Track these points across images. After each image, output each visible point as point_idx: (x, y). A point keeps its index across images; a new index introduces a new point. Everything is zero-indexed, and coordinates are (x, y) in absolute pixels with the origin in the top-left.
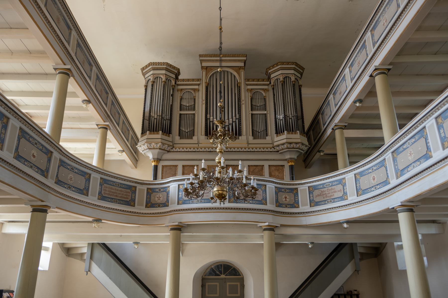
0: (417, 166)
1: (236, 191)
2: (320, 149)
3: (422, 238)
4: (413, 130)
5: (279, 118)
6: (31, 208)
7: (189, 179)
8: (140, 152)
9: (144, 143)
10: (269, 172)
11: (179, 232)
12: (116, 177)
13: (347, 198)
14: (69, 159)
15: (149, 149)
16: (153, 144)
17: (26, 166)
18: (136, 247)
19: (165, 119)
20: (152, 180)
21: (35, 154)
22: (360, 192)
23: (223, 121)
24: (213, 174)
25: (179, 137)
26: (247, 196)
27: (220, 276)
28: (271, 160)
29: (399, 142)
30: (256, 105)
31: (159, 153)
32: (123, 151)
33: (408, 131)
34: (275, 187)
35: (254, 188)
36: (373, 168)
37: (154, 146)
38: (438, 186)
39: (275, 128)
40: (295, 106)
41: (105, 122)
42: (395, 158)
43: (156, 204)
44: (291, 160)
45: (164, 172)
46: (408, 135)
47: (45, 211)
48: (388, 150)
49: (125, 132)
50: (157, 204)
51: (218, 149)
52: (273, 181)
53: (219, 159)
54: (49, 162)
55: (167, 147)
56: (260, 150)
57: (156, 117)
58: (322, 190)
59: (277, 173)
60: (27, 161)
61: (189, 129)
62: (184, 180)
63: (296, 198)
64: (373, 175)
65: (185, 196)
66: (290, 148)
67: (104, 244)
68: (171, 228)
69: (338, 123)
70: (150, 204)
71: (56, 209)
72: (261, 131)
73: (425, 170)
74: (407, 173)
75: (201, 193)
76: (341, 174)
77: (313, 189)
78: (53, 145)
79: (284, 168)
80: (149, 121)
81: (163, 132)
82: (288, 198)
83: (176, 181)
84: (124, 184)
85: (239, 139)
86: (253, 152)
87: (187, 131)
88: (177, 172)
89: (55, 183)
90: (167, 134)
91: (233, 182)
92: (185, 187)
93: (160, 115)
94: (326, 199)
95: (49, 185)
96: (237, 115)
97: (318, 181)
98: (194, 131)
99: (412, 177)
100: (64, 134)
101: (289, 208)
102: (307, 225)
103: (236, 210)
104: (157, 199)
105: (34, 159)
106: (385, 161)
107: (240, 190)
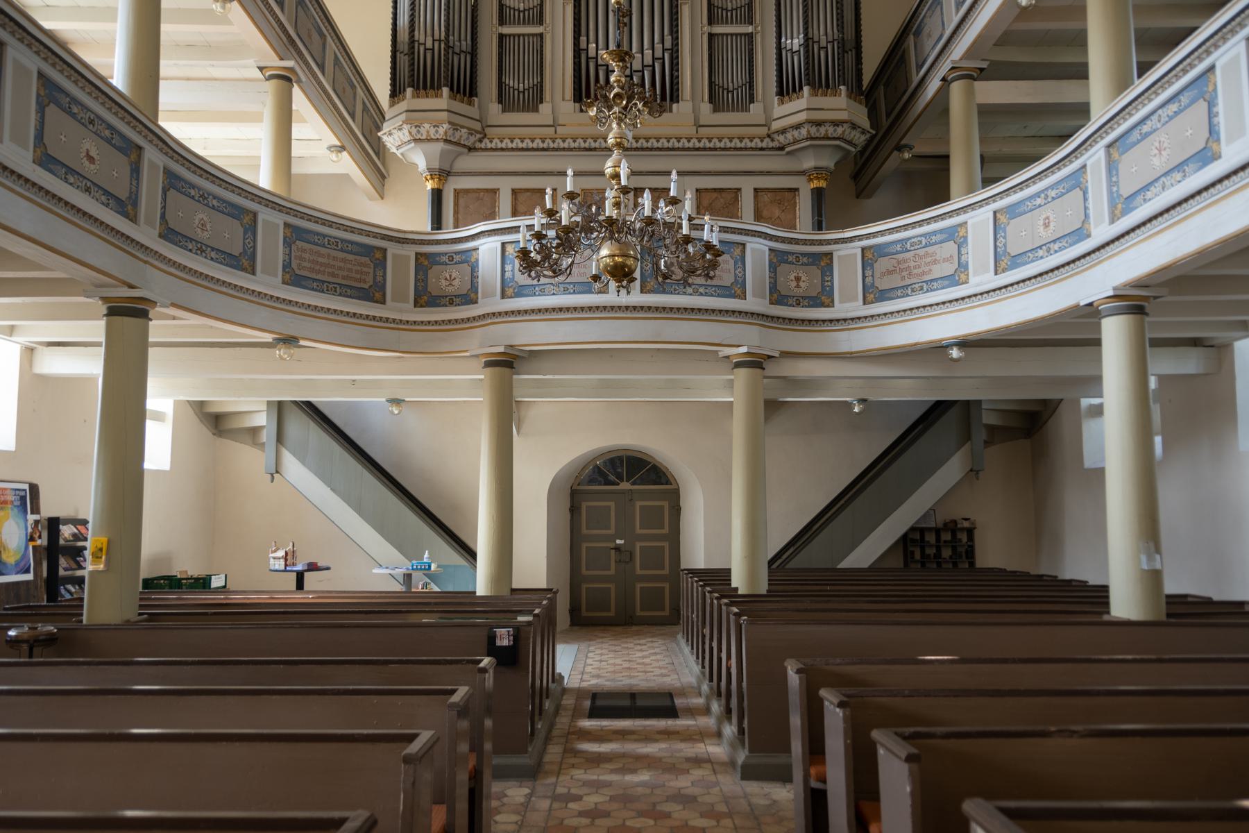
0: (1172, 185)
1: (661, 257)
2: (903, 142)
3: (1157, 387)
4: (1178, 77)
5: (789, 47)
6: (103, 304)
7: (532, 227)
8: (392, 151)
9: (401, 123)
10: (755, 207)
11: (507, 370)
12: (326, 222)
13: (968, 279)
14: (192, 170)
15: (416, 140)
16: (427, 126)
17: (74, 187)
18: (396, 412)
19: (457, 50)
20: (429, 229)
21: (93, 153)
22: (1005, 261)
23: (626, 53)
24: (598, 208)
25: (500, 105)
26: (692, 272)
27: (618, 484)
28: (761, 173)
29: (1133, 115)
30: (724, 7)
31: (443, 154)
32: (343, 148)
33: (1163, 81)
34: (770, 250)
35: (711, 248)
36: (1049, 194)
37: (428, 132)
38: (1224, 241)
39: (775, 78)
40: (837, 9)
41: (282, 59)
42: (1114, 162)
43: (443, 297)
44: (817, 174)
45: (461, 210)
46: (1160, 91)
47: (143, 314)
48: (1101, 134)
49: (344, 92)
50: (446, 296)
51: (611, 136)
52: (766, 233)
53: (615, 167)
54: (135, 175)
55: (465, 136)
56: (732, 145)
57: (429, 45)
58: (900, 256)
59: (777, 212)
60: (73, 172)
61: (526, 82)
62: (516, 229)
63: (827, 279)
64: (1047, 212)
65: (521, 271)
66: (817, 138)
67: (309, 404)
68: (485, 362)
69: (961, 59)
70: (425, 298)
71: (171, 308)
72: (736, 87)
73: (1192, 196)
74: (1141, 205)
75: (564, 264)
76: (957, 211)
77: (874, 256)
78: (140, 126)
79: (797, 198)
80: (412, 57)
81: (452, 89)
82: (804, 280)
83: (496, 232)
84: (352, 243)
85: (671, 111)
86: (710, 149)
87: (521, 89)
88: (497, 209)
89: (161, 236)
90: (466, 98)
91: (653, 231)
92: (521, 246)
93: (443, 38)
94: (908, 282)
95: (119, 229)
96: (665, 38)
97: (891, 231)
98: (542, 86)
99: (1155, 217)
100: (168, 96)
101: (806, 307)
102: (852, 353)
103: (660, 312)
104: (444, 283)
105: (92, 167)
106: (1085, 173)
107: (672, 253)
